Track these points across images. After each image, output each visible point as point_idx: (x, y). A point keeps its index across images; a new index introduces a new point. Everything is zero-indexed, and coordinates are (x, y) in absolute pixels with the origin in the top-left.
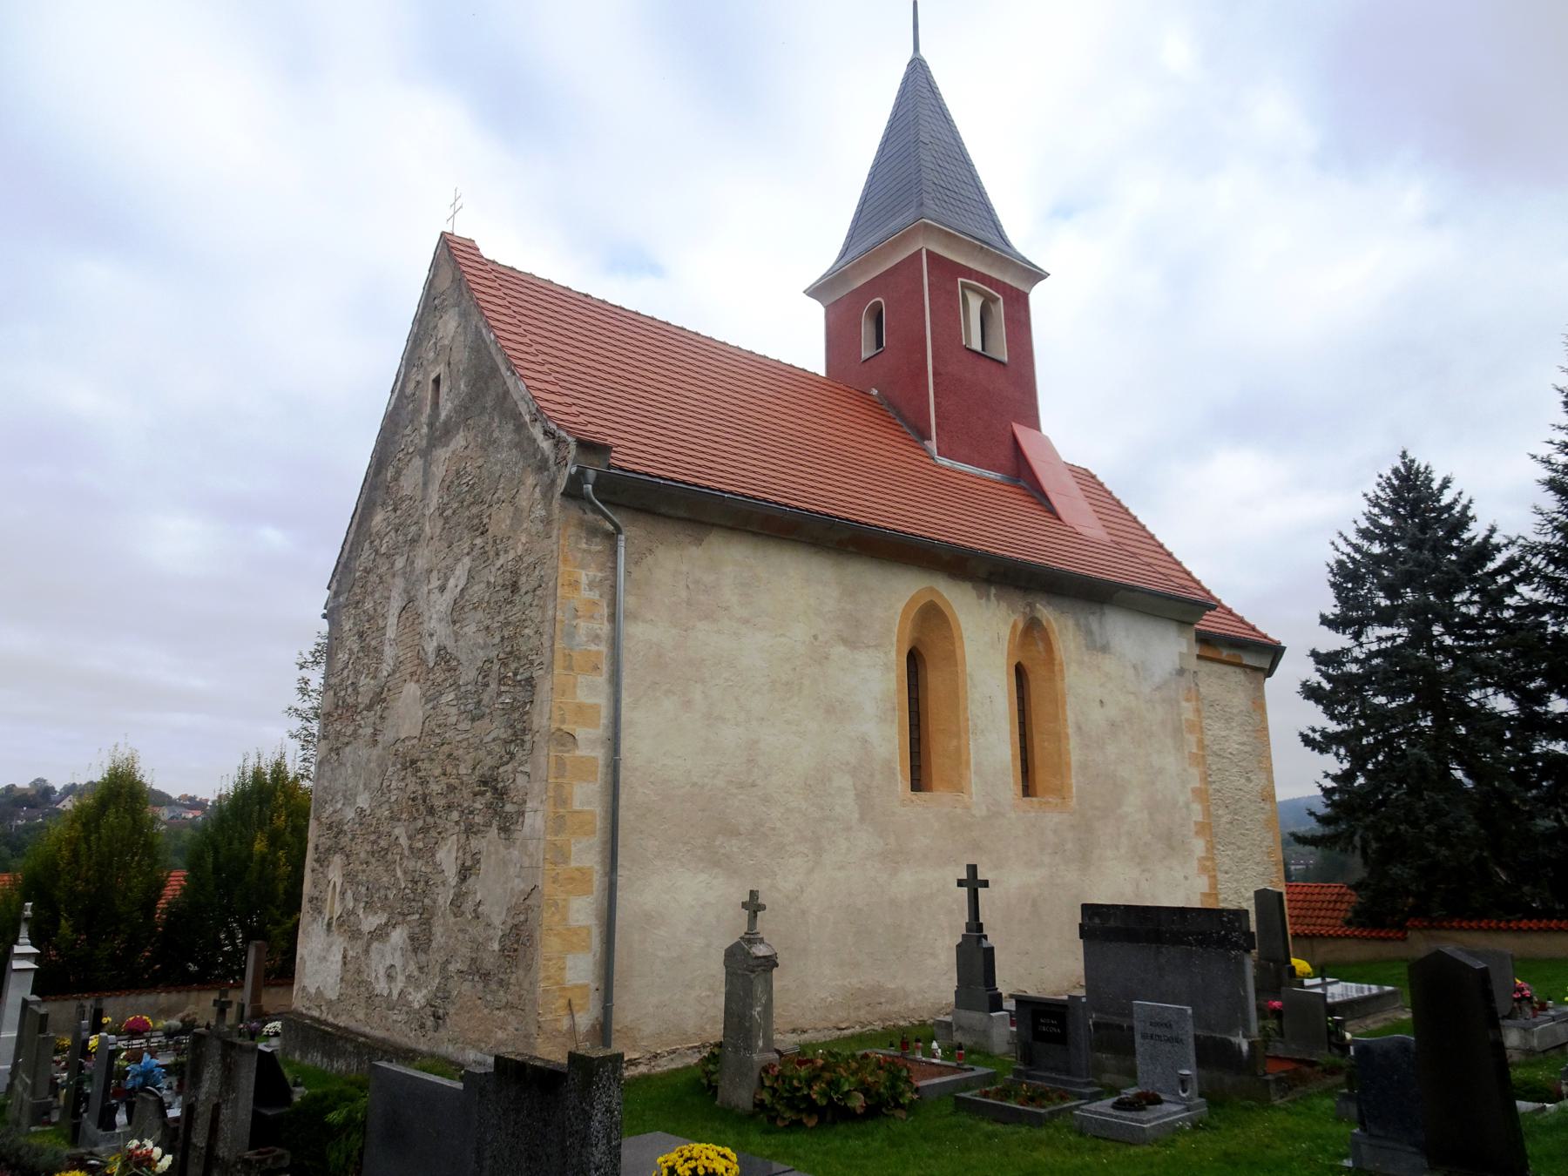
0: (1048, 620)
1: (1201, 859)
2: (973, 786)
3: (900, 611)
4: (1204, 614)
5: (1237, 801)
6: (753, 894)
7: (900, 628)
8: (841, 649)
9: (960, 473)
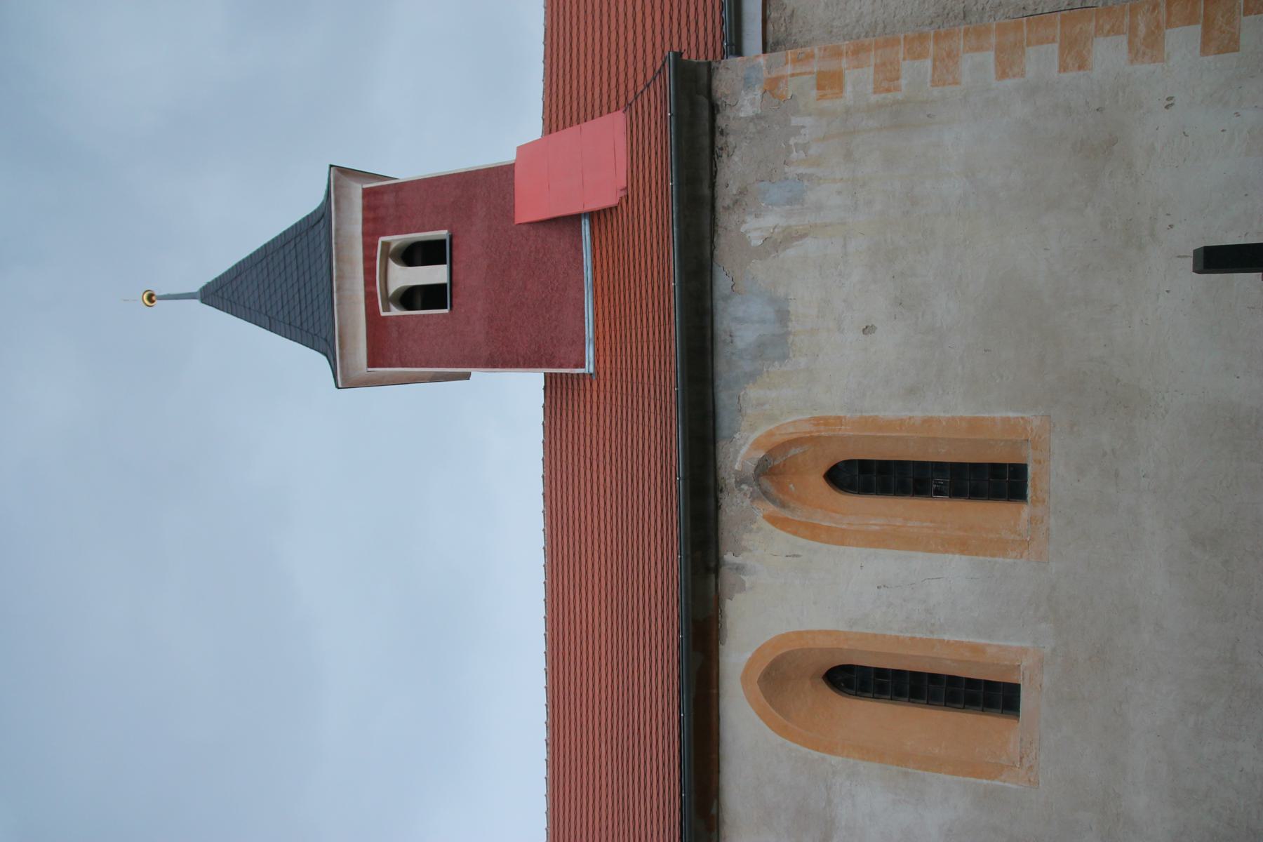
1: (1135, 54)
2: (1010, 644)
3: (780, 739)
4: (689, 63)
7: (805, 745)
9: (594, 256)
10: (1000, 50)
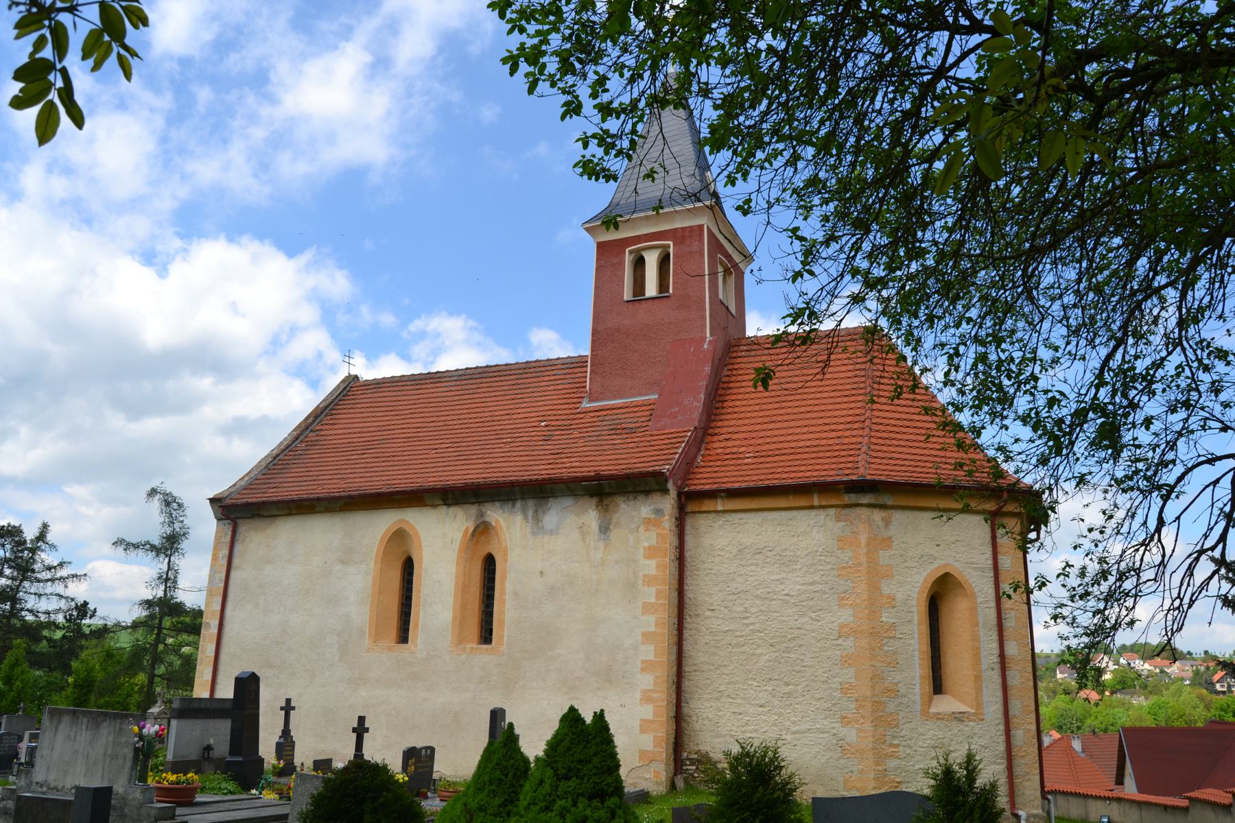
0: (497, 521)
1: (645, 692)
5: (793, 639)
6: (288, 701)
8: (340, 567)
10: (654, 633)
